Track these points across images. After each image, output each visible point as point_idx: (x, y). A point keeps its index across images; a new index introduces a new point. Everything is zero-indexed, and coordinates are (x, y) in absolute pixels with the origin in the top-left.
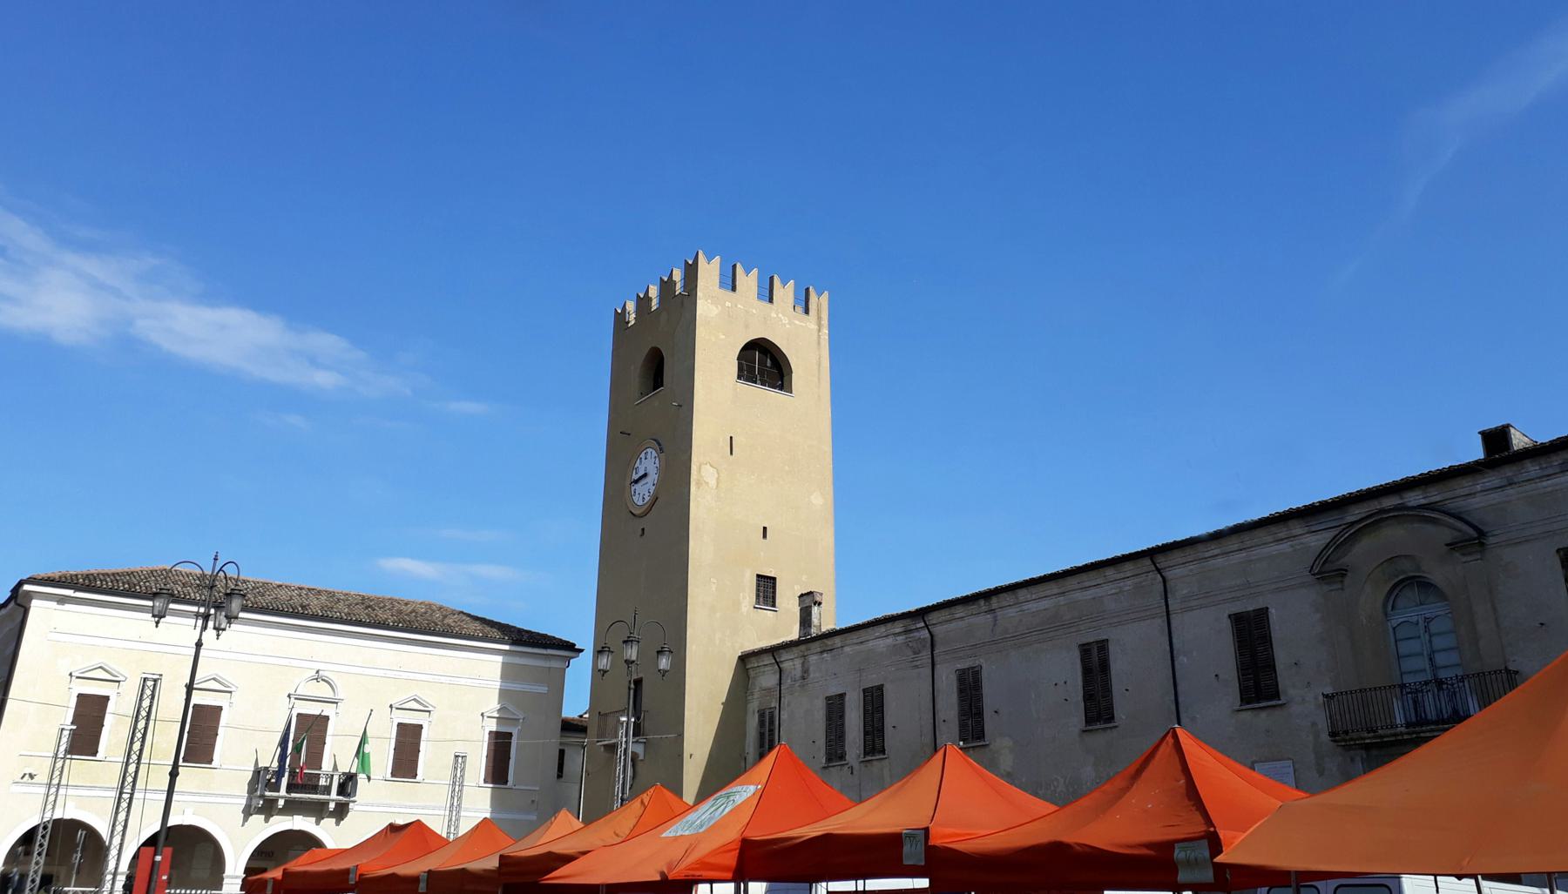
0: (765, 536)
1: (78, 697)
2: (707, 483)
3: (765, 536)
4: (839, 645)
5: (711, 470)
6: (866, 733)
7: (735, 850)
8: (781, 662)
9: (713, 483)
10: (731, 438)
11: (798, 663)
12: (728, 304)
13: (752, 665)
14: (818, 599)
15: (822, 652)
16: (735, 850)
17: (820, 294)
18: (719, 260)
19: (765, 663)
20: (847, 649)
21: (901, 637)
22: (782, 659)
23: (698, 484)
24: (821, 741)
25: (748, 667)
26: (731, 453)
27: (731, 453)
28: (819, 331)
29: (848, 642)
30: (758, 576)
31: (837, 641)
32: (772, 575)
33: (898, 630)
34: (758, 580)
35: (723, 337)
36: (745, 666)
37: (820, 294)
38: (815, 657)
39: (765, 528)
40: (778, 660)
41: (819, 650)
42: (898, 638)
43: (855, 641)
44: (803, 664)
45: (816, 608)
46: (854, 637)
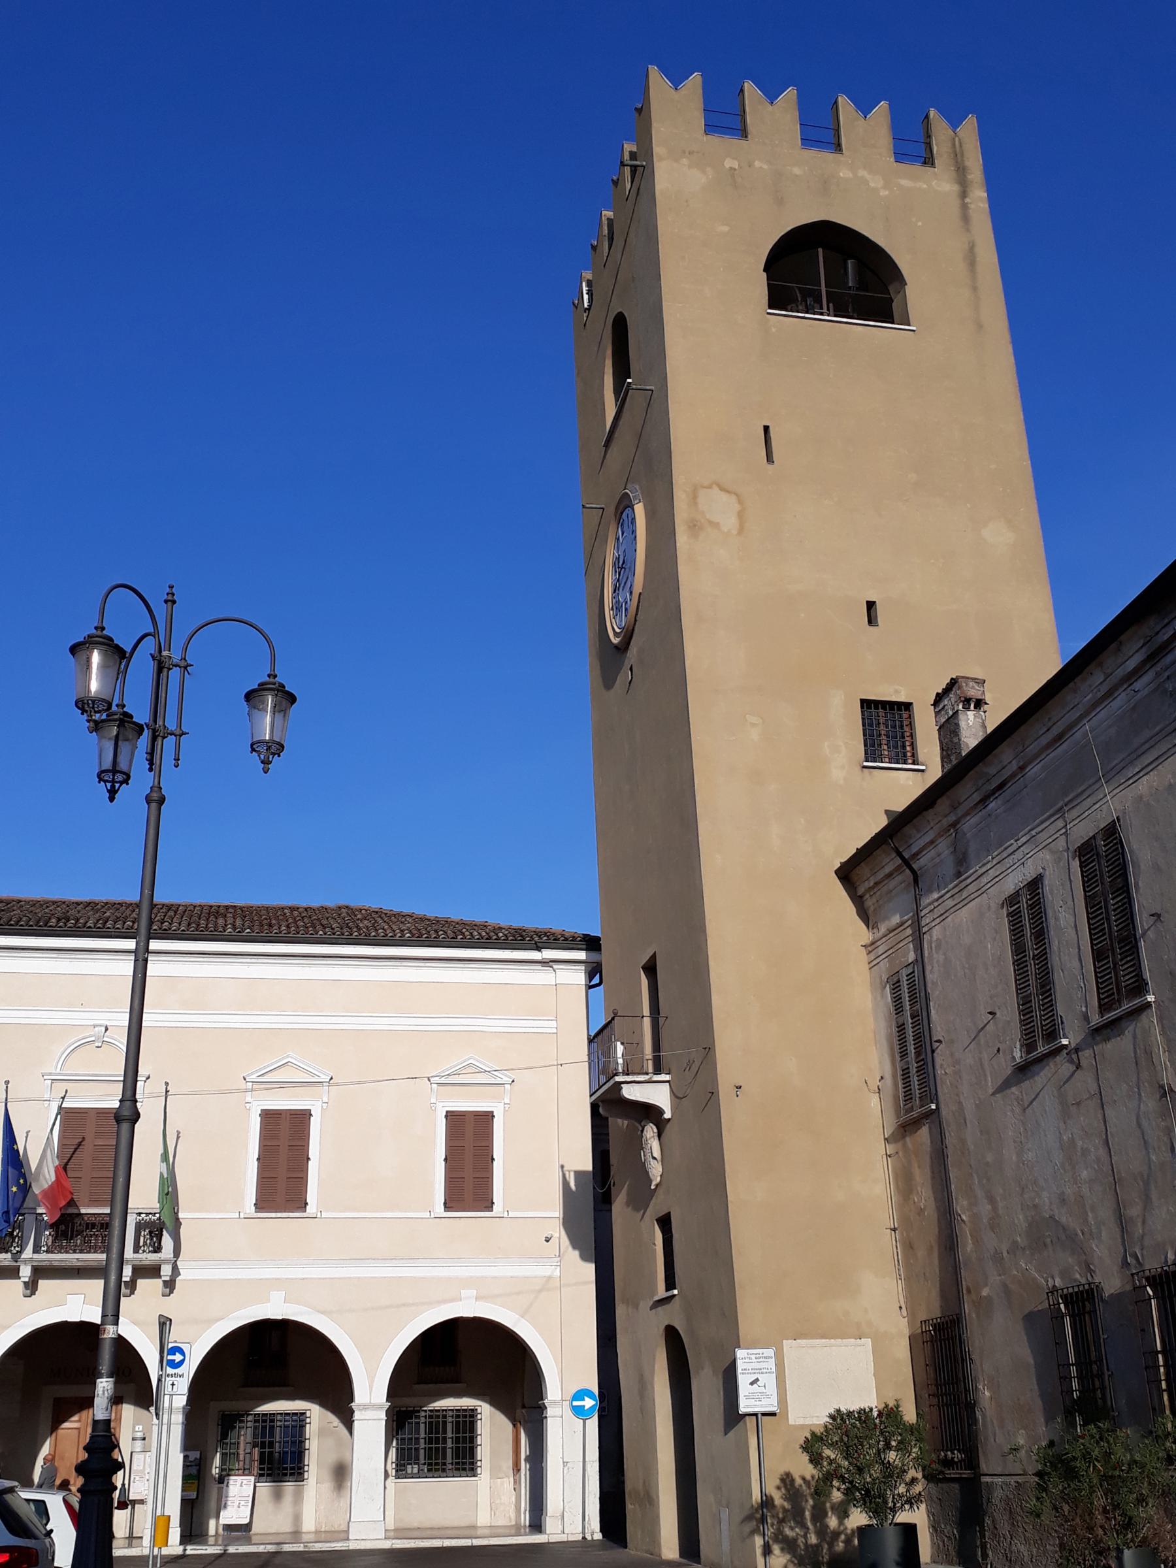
0: (872, 620)
1: (446, 1116)
2: (716, 525)
3: (872, 620)
4: (1014, 766)
5: (724, 497)
6: (1098, 955)
7: (63, 1429)
8: (915, 855)
9: (729, 522)
10: (766, 429)
11: (944, 847)
12: (729, 163)
13: (867, 885)
14: (973, 692)
15: (984, 801)
16: (63, 1429)
17: (955, 123)
18: (699, 79)
19: (887, 870)
20: (1034, 770)
21: (1146, 679)
22: (914, 849)
23: (695, 527)
24: (1010, 1012)
25: (860, 891)
26: (770, 458)
27: (770, 458)
28: (964, 194)
29: (1033, 748)
30: (866, 704)
31: (1006, 757)
32: (902, 698)
33: (1131, 664)
34: (862, 707)
35: (726, 229)
36: (856, 892)
37: (955, 123)
38: (973, 820)
39: (871, 605)
40: (906, 855)
41: (977, 797)
42: (1137, 685)
43: (1045, 740)
44: (955, 846)
45: (971, 714)
46: (1037, 733)
